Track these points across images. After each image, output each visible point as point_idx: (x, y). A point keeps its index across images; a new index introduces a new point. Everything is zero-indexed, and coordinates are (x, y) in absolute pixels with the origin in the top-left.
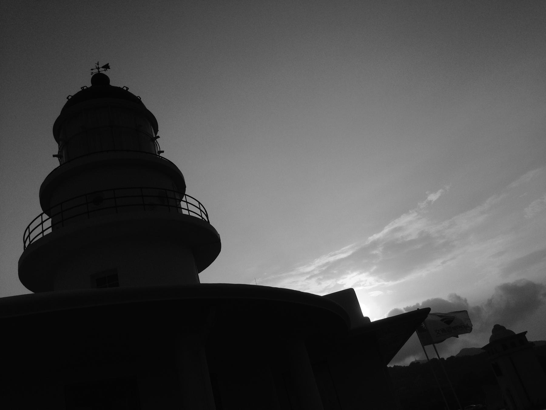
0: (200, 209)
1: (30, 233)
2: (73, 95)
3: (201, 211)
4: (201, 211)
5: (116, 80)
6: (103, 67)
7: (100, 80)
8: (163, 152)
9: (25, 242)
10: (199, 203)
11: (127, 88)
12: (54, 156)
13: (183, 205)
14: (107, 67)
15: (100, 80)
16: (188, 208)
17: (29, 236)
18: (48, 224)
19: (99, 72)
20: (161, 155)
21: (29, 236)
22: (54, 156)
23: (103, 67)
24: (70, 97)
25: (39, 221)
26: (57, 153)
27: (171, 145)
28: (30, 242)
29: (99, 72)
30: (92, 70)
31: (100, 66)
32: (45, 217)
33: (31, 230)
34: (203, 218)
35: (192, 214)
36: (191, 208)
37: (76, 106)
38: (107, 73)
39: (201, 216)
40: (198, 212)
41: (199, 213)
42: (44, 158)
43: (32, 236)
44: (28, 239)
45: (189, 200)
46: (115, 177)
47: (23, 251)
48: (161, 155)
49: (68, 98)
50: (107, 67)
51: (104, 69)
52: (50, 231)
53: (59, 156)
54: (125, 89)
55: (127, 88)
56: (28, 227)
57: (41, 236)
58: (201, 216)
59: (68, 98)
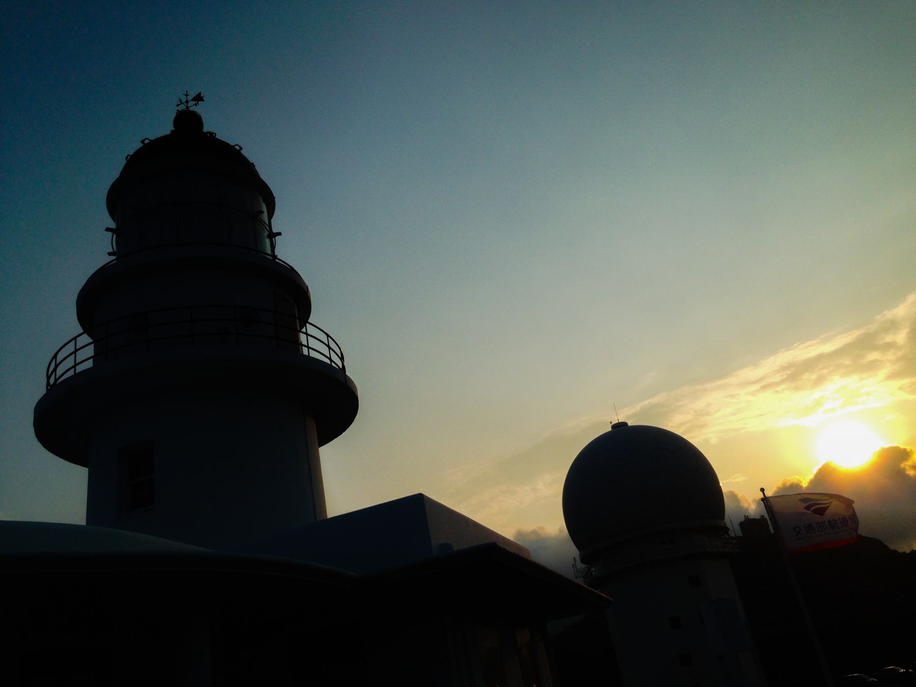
0: (328, 346)
1: (57, 366)
2: (152, 138)
5: (218, 123)
6: (193, 100)
7: (188, 121)
8: (108, 229)
9: (48, 378)
10: (328, 336)
11: (241, 148)
12: (280, 234)
13: (303, 338)
14: (199, 98)
15: (188, 121)
16: (314, 346)
17: (55, 370)
18: (90, 351)
19: (187, 107)
20: (113, 225)
22: (280, 234)
23: (193, 100)
24: (146, 141)
25: (70, 348)
26: (278, 238)
27: (295, 243)
28: (56, 380)
29: (187, 107)
30: (178, 105)
31: (190, 98)
32: (85, 339)
33: (59, 360)
34: (331, 361)
35: (313, 354)
36: (313, 343)
37: (146, 162)
38: (200, 109)
39: (330, 359)
40: (325, 350)
41: (327, 353)
42: (90, 245)
43: (60, 371)
44: (53, 376)
45: (310, 330)
46: (206, 330)
47: (43, 391)
48: (113, 225)
49: (143, 142)
50: (199, 98)
52: (89, 364)
53: (273, 235)
54: (237, 148)
55: (241, 148)
56: (55, 356)
57: (71, 373)
58: (330, 359)
59: (143, 142)
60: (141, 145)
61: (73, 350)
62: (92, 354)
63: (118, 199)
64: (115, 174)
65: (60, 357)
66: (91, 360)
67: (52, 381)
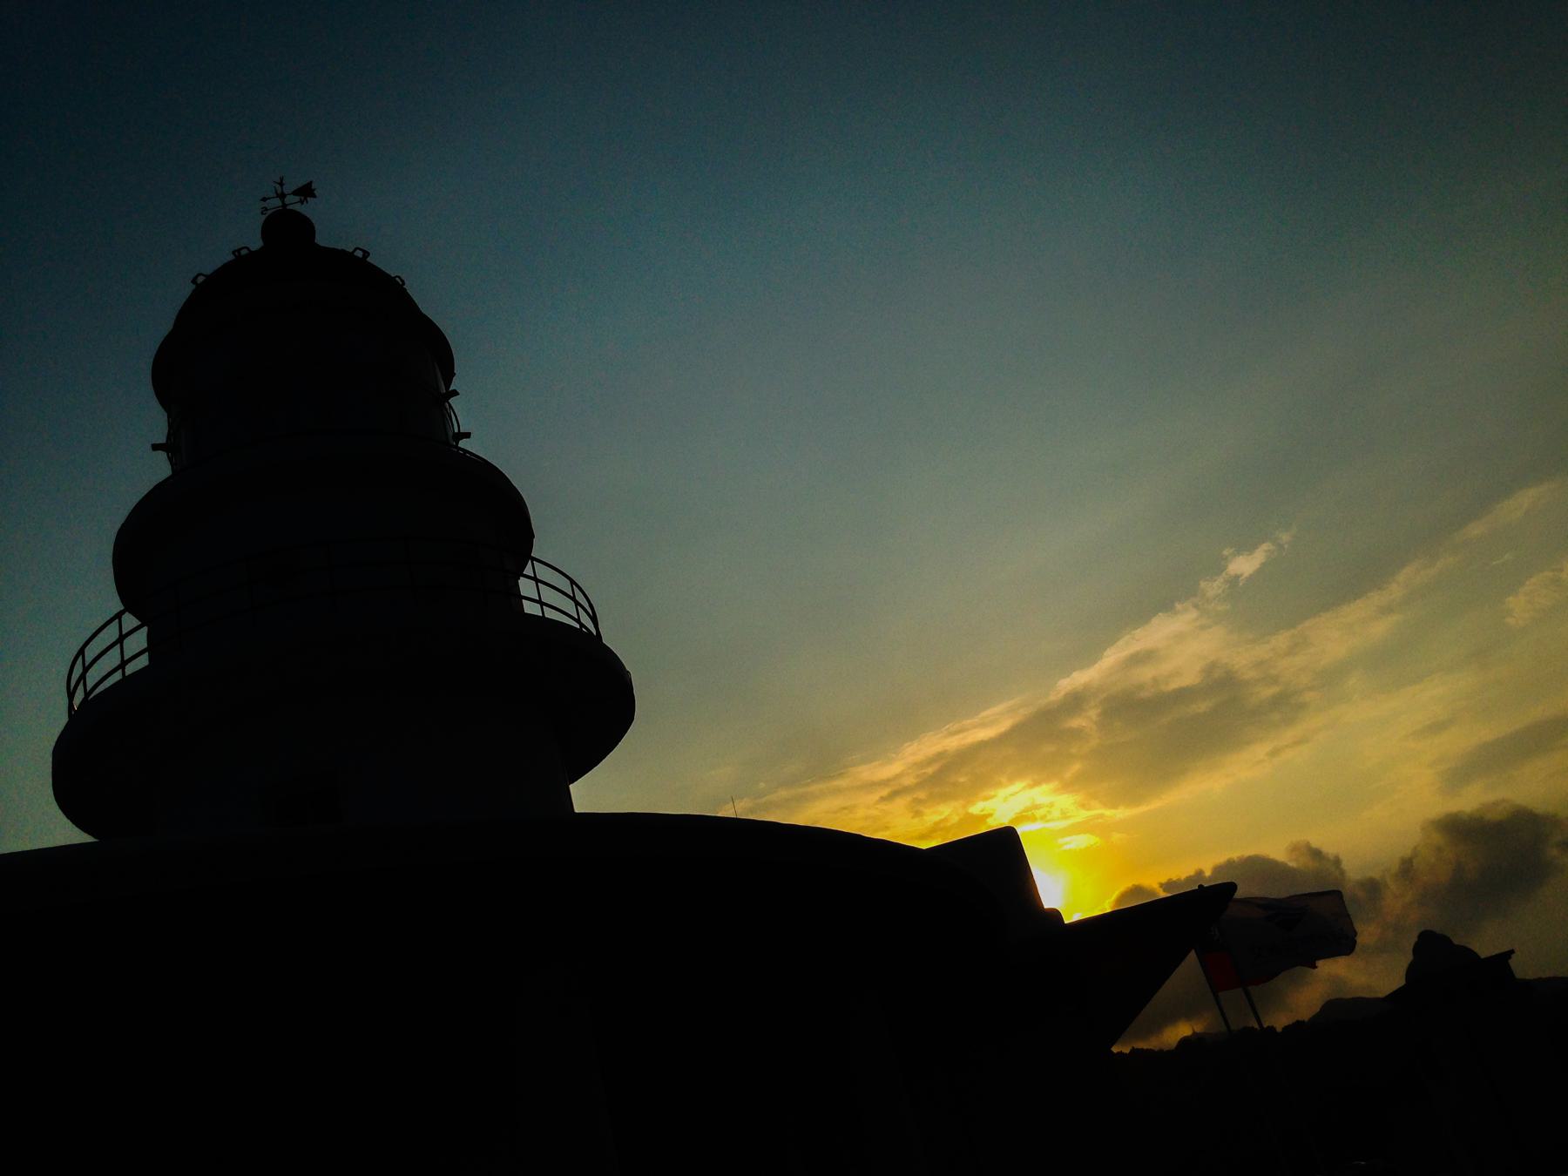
0: (573, 598)
1: (86, 669)
2: (208, 271)
3: (577, 604)
4: (577, 604)
5: (336, 226)
6: (295, 193)
7: (287, 228)
8: (467, 435)
9: (71, 695)
10: (573, 582)
11: (366, 254)
13: (526, 587)
14: (306, 192)
15: (287, 228)
17: (83, 677)
18: (139, 641)
19: (284, 205)
21: (83, 677)
23: (295, 193)
24: (200, 279)
25: (111, 633)
27: (490, 418)
28: (87, 694)
31: (288, 189)
32: (130, 621)
33: (88, 660)
34: (582, 625)
35: (550, 614)
36: (549, 596)
37: (217, 305)
38: (308, 209)
39: (578, 621)
40: (569, 607)
41: (571, 609)
42: (129, 456)
43: (93, 677)
44: (81, 686)
45: (543, 573)
46: (345, 559)
49: (194, 281)
50: (306, 192)
51: (297, 198)
52: (143, 661)
54: (359, 254)
55: (366, 254)
56: (81, 652)
57: (117, 676)
58: (578, 621)
59: (194, 281)
60: (231, 257)
61: (116, 636)
62: (145, 645)
63: (170, 374)
64: (166, 327)
65: (90, 654)
66: (146, 656)
67: (79, 697)
